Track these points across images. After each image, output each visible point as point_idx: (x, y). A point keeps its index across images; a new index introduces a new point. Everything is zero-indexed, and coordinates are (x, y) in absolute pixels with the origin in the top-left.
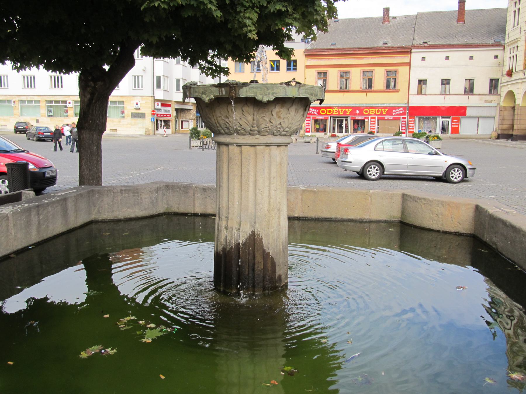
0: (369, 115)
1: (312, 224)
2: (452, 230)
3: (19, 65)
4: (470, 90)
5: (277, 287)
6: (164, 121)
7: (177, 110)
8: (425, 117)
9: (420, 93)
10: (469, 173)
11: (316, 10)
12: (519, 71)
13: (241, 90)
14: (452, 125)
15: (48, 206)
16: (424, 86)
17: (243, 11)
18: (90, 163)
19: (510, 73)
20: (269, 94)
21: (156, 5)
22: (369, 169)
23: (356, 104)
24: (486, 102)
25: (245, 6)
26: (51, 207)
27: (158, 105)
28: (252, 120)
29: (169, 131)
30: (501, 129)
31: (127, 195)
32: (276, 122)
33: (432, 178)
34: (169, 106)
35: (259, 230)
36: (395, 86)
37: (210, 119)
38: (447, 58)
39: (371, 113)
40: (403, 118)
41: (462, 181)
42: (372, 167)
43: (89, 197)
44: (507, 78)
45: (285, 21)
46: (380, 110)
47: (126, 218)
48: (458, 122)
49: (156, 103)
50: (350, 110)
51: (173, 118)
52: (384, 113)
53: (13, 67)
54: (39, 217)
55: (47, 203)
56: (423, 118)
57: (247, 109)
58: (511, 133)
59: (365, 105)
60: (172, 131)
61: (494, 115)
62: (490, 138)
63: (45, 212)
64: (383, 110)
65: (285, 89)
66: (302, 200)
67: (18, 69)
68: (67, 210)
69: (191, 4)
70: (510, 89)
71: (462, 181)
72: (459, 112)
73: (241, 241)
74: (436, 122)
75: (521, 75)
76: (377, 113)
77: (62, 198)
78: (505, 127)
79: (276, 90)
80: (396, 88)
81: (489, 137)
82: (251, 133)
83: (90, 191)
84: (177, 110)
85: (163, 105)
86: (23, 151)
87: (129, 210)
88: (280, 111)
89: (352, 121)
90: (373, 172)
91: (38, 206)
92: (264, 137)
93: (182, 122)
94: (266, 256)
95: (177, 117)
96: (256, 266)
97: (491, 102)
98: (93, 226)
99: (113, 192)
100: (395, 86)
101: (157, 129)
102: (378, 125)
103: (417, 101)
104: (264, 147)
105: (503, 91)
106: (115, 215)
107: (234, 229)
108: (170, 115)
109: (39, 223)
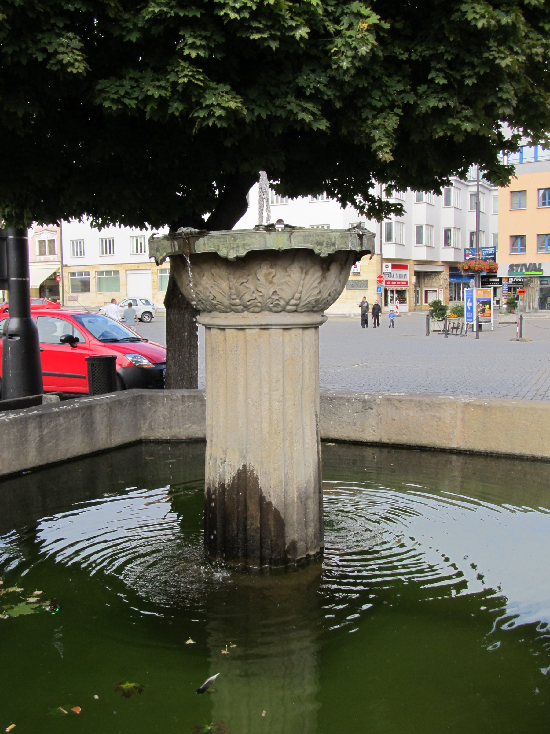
1: (479, 463)
3: (100, 221)
5: (289, 561)
6: (398, 292)
7: (418, 274)
11: (501, 99)
13: (197, 243)
15: (59, 416)
17: (370, 116)
18: (179, 356)
20: (238, 247)
21: (211, 124)
25: (374, 108)
26: (64, 418)
27: (387, 266)
28: (227, 288)
29: (404, 308)
31: (191, 403)
32: (267, 290)
34: (405, 267)
35: (252, 464)
43: (135, 405)
45: (447, 124)
47: (190, 439)
49: (384, 264)
51: (410, 288)
53: (92, 224)
54: (41, 431)
55: (57, 412)
57: (218, 271)
60: (410, 307)
63: (53, 424)
65: (265, 238)
66: (463, 420)
67: (100, 227)
68: (93, 423)
69: (278, 114)
73: (228, 480)
77: (84, 405)
79: (248, 240)
82: (232, 309)
83: (138, 396)
84: (418, 274)
85: (394, 267)
86: (138, 340)
87: (194, 426)
88: (270, 273)
91: (40, 416)
92: (256, 315)
93: (426, 292)
94: (264, 505)
95: (418, 284)
96: (249, 523)
98: (143, 448)
99: (172, 399)
101: (386, 305)
104: (258, 330)
106: (173, 434)
107: (218, 460)
108: (407, 282)
109: (41, 439)
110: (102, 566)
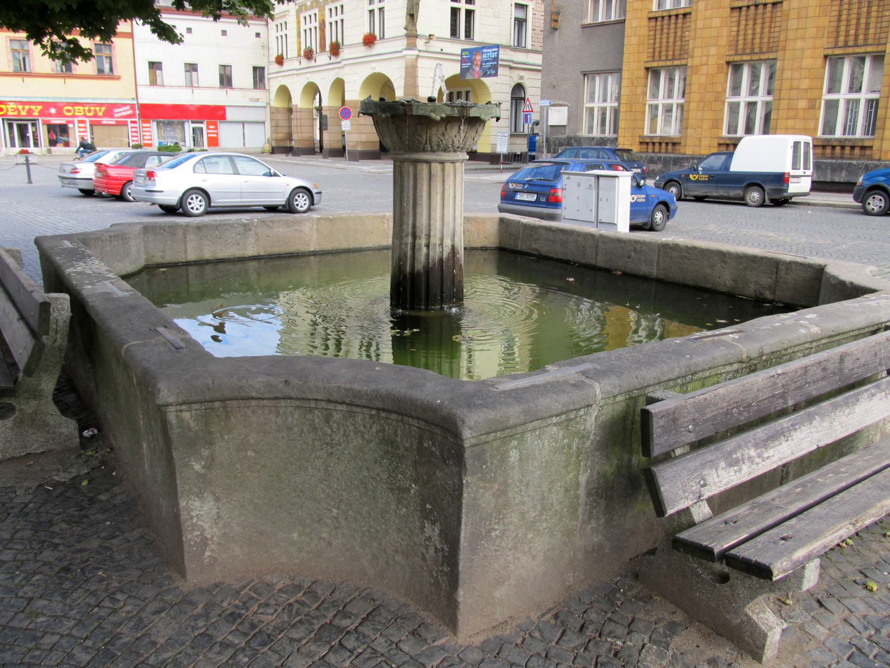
0: (74, 116)
1: (330, 258)
2: (479, 245)
4: (226, 80)
8: (166, 121)
9: (153, 82)
10: (316, 197)
12: (292, 59)
14: (208, 133)
16: (158, 72)
19: (280, 60)
22: (189, 200)
23: (47, 98)
24: (251, 100)
30: (276, 140)
33: (262, 208)
36: (111, 69)
37: (420, 136)
38: (224, 33)
39: (76, 114)
40: (132, 122)
41: (309, 210)
42: (194, 196)
44: (276, 67)
46: (92, 108)
48: (216, 128)
50: (40, 107)
52: (100, 114)
56: (163, 123)
58: (288, 145)
59: (64, 101)
61: (264, 119)
62: (263, 153)
64: (98, 109)
66: (317, 230)
70: (282, 84)
71: (309, 210)
72: (215, 114)
74: (184, 128)
75: (295, 65)
76: (88, 114)
78: (280, 136)
80: (115, 73)
81: (259, 150)
89: (46, 127)
90: (196, 205)
97: (258, 100)
100: (111, 69)
102: (92, 133)
103: (151, 96)
105: (273, 85)
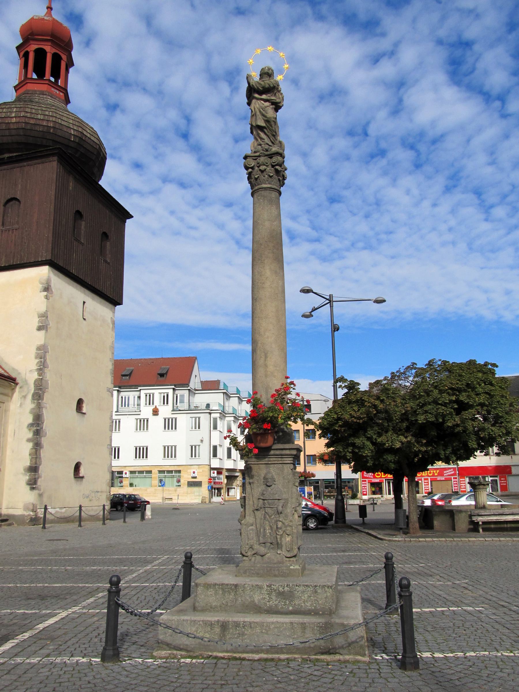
7: (227, 477)
27: (214, 473)
49: (212, 471)
110: (270, 656)
